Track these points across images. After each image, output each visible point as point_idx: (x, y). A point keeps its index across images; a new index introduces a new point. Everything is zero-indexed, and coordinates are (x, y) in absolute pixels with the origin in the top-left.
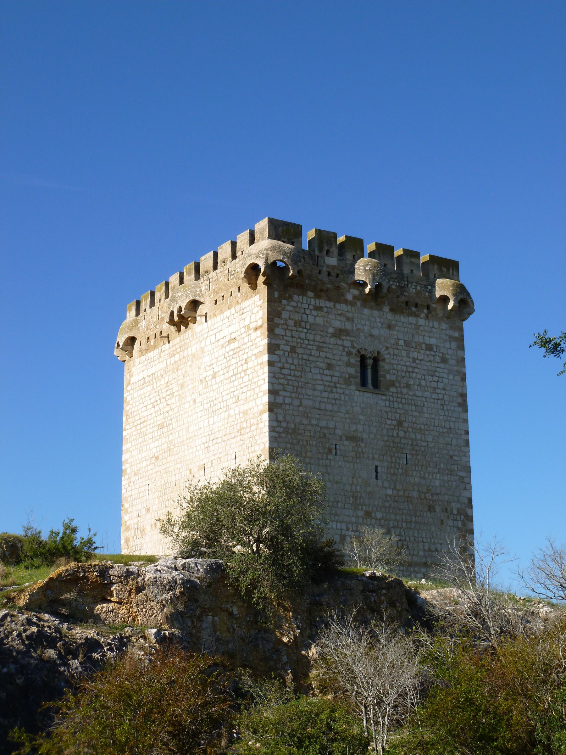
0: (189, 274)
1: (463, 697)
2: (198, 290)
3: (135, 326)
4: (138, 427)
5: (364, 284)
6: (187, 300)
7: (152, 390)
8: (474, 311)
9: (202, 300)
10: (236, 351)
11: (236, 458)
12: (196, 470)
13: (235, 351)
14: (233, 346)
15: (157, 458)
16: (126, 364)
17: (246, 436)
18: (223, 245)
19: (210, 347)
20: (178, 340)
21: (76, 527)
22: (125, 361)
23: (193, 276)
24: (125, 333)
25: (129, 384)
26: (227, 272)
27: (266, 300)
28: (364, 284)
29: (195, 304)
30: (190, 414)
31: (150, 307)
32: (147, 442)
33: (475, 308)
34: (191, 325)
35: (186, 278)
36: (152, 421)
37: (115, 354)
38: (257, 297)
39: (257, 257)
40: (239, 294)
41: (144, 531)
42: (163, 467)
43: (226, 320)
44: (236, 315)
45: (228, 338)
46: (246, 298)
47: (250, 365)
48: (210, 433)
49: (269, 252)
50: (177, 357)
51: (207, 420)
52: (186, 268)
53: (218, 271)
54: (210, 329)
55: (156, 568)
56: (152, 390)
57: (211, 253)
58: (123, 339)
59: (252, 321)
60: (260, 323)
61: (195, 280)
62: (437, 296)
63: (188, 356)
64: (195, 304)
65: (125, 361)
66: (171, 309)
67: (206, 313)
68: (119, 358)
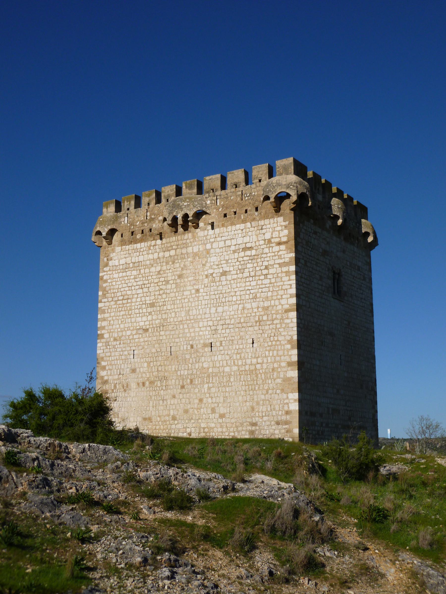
0: (190, 187)
1: (83, 512)
2: (204, 203)
3: (116, 221)
4: (119, 302)
5: (337, 217)
6: (195, 210)
7: (139, 275)
8: (378, 245)
9: (208, 212)
10: (252, 258)
11: (253, 343)
12: (199, 346)
13: (251, 258)
14: (248, 253)
15: (146, 330)
16: (102, 250)
17: (267, 327)
18: (234, 171)
19: (218, 250)
20: (171, 239)
21: (422, 419)
22: (101, 247)
23: (195, 191)
24: (108, 225)
25: (107, 265)
26: (240, 193)
27: (293, 223)
28: (337, 217)
29: (199, 215)
30: (191, 300)
31: (135, 208)
32: (132, 316)
33: (379, 243)
34: (191, 229)
35: (184, 190)
36: (139, 300)
37: (93, 239)
38: (281, 219)
39: (288, 187)
40: (256, 213)
41: (127, 386)
42: (155, 338)
43: (240, 231)
44: (252, 229)
45: (243, 246)
46: (266, 217)
47: (272, 271)
48: (219, 318)
49: (298, 185)
50: (173, 253)
51: (215, 308)
52: (186, 184)
53: (227, 191)
54: (217, 236)
55: (345, 443)
56: (139, 275)
57: (219, 176)
58: (106, 230)
59: (274, 236)
60: (285, 239)
61: (197, 194)
62: (363, 232)
63: (187, 253)
64: (199, 215)
65: (101, 247)
66: (175, 214)
67: (213, 223)
68: (96, 244)
